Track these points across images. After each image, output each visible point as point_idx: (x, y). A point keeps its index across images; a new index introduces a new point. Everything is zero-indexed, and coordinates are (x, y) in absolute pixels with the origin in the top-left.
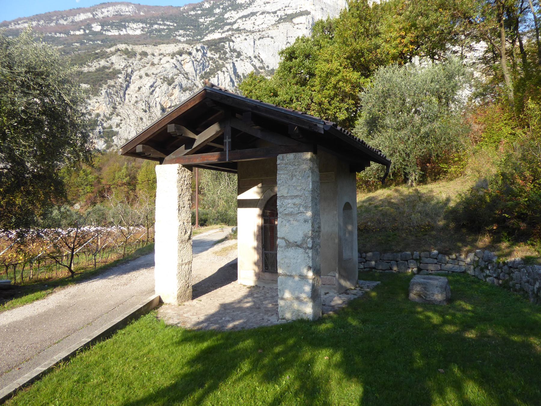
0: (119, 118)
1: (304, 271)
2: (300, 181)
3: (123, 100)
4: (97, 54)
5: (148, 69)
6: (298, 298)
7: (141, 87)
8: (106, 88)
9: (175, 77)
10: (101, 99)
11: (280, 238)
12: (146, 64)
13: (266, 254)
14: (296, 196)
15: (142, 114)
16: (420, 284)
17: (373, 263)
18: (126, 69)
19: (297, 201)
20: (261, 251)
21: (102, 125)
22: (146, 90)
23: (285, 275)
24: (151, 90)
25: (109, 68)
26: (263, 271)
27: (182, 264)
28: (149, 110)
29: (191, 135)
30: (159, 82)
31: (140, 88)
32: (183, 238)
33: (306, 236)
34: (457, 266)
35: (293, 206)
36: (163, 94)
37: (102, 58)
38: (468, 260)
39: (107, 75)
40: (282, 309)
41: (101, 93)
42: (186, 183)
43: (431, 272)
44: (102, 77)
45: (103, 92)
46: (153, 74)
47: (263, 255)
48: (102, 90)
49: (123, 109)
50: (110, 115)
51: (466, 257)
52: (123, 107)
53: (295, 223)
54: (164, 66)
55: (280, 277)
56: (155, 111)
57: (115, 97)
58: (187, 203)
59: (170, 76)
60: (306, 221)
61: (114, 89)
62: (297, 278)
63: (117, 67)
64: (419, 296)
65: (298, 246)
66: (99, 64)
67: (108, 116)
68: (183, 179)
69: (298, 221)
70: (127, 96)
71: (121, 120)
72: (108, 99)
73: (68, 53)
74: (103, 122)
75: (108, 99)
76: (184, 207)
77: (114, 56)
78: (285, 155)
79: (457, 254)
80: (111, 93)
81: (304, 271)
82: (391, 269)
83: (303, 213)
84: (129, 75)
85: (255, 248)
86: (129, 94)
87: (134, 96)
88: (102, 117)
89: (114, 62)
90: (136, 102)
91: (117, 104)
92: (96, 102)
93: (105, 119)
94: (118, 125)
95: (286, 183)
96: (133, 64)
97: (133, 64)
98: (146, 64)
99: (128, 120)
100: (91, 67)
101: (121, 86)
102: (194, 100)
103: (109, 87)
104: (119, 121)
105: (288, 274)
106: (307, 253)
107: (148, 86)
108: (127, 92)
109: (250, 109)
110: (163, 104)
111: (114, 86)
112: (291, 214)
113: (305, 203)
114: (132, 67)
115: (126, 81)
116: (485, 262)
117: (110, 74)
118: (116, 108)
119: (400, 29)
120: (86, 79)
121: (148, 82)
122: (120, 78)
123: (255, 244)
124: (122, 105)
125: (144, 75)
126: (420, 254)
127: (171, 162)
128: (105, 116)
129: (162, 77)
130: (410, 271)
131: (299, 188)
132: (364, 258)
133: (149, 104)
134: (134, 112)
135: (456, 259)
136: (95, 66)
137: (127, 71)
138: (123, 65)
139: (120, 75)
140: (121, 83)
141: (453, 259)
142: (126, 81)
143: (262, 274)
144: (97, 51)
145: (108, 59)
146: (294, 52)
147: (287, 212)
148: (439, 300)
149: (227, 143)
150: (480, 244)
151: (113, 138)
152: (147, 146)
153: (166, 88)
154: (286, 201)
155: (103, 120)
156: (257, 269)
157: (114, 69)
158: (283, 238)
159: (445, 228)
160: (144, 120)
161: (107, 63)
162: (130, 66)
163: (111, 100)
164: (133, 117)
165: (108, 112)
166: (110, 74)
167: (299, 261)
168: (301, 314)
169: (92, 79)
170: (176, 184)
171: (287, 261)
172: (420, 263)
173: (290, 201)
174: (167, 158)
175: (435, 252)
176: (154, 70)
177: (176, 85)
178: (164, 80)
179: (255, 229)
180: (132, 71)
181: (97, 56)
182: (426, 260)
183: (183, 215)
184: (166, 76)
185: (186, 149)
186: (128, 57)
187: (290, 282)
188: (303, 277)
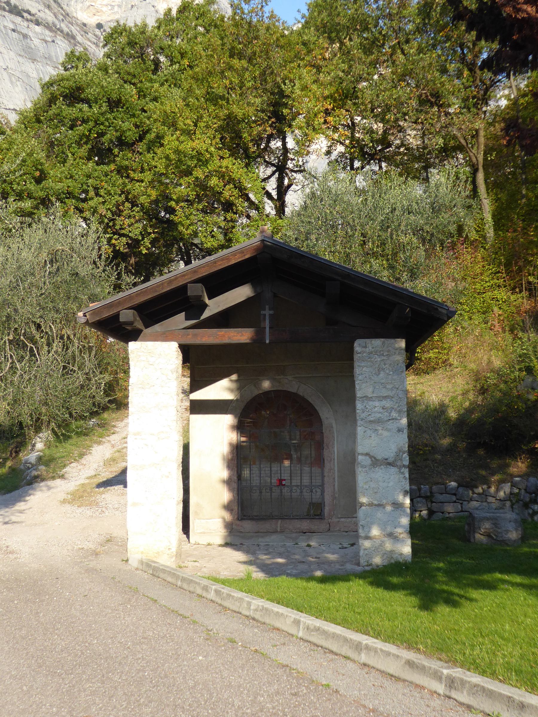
1: (401, 498)
2: (390, 377)
6: (391, 535)
11: (362, 454)
14: (385, 398)
16: (488, 519)
19: (388, 404)
20: (235, 485)
23: (371, 505)
26: (238, 519)
33: (400, 450)
34: (485, 504)
35: (381, 410)
38: (501, 494)
40: (366, 552)
43: (447, 515)
51: (498, 490)
53: (386, 433)
55: (363, 508)
60: (400, 430)
62: (389, 508)
64: (489, 536)
65: (390, 464)
69: (388, 430)
78: (368, 341)
79: (485, 487)
81: (401, 498)
83: (396, 419)
85: (224, 482)
95: (370, 378)
102: (242, 252)
105: (376, 502)
106: (403, 473)
109: (340, 278)
112: (379, 421)
113: (399, 407)
116: (531, 494)
119: (325, 98)
123: (225, 474)
126: (431, 488)
127: (165, 337)
130: (417, 515)
131: (389, 387)
135: (483, 494)
141: (479, 494)
143: (238, 522)
146: (80, 89)
147: (372, 419)
149: (267, 317)
150: (513, 470)
154: (371, 403)
156: (227, 516)
158: (367, 454)
159: (451, 449)
167: (391, 484)
168: (395, 556)
171: (372, 485)
172: (432, 502)
173: (377, 404)
174: (147, 331)
175: (453, 484)
179: (225, 449)
182: (441, 498)
185: (187, 319)
187: (379, 514)
188: (397, 506)
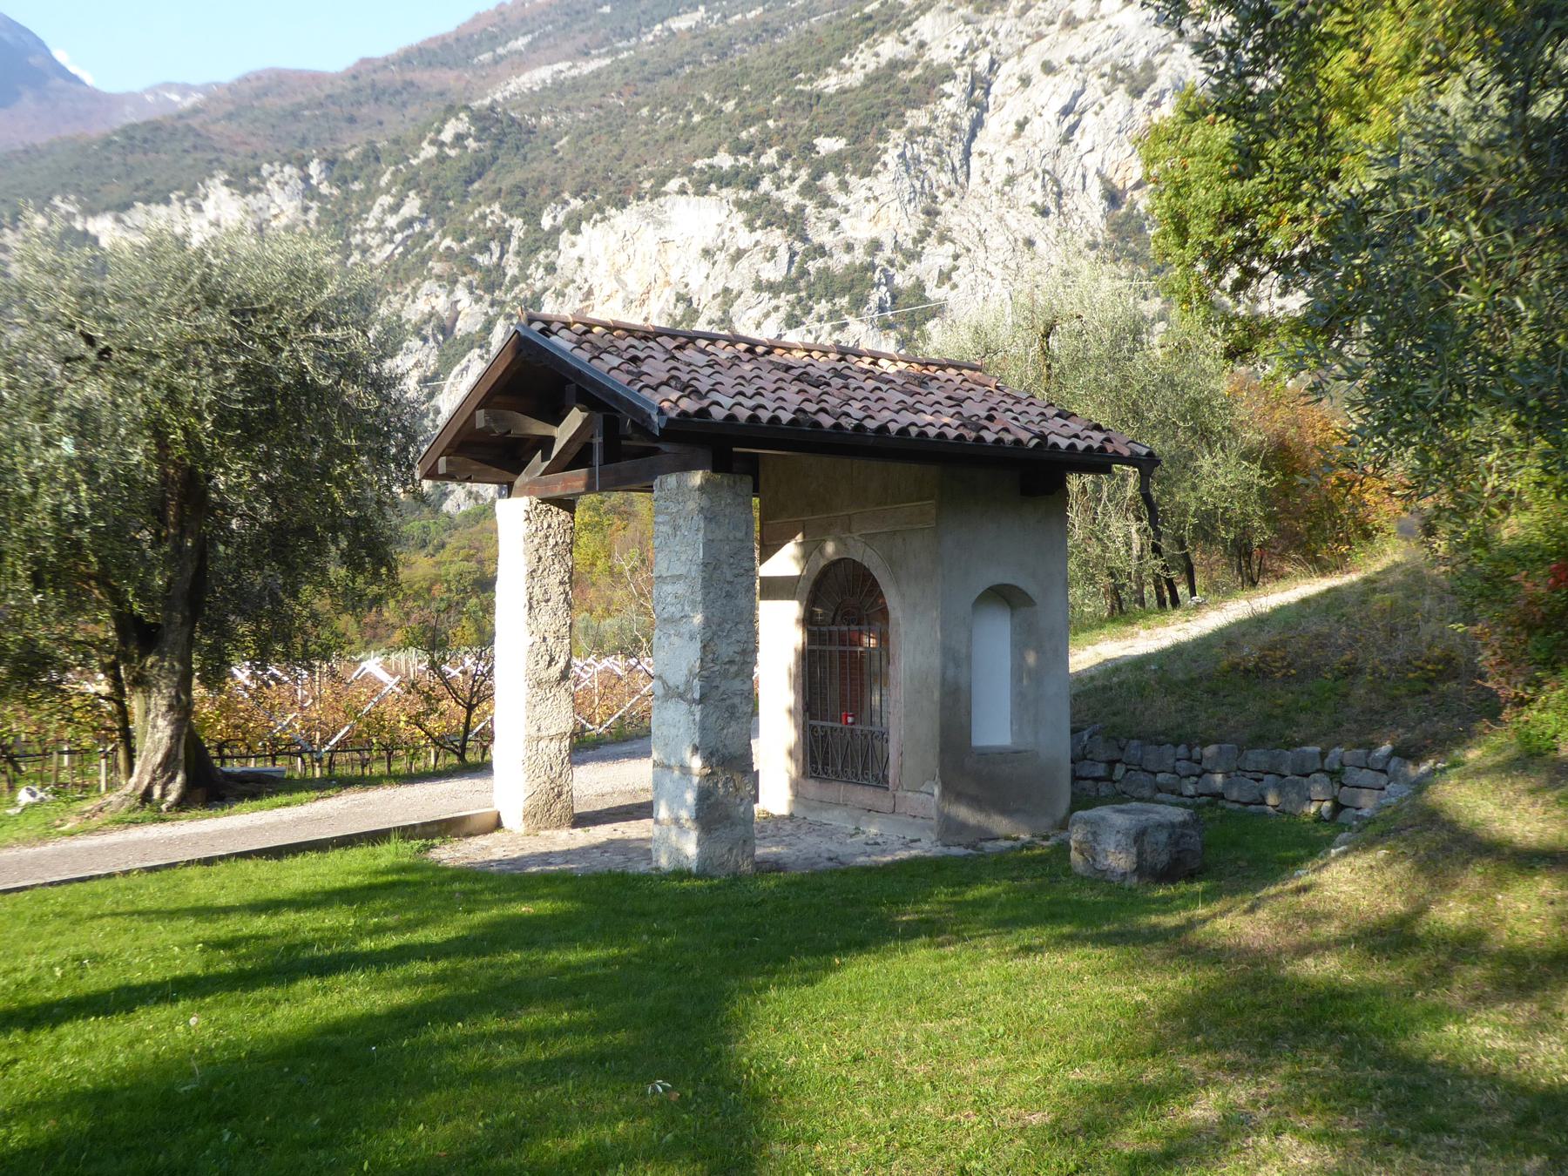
0: (949, 248)
1: (687, 754)
3: (962, 179)
4: (869, 18)
5: (1053, 46)
7: (1026, 120)
8: (901, 141)
9: (1158, 59)
10: (882, 183)
12: (1043, 28)
13: (813, 728)
15: (1031, 225)
17: (1219, 778)
18: (970, 59)
19: (680, 588)
21: (889, 279)
22: (1045, 130)
24: (1065, 126)
25: (908, 65)
27: (539, 739)
28: (1059, 206)
29: (538, 428)
30: (1096, 87)
31: (1021, 126)
32: (544, 675)
36: (1112, 135)
37: (886, 32)
39: (905, 91)
41: (885, 164)
42: (552, 541)
44: (887, 103)
45: (891, 157)
46: (1071, 61)
47: (804, 731)
48: (885, 151)
49: (963, 213)
50: (915, 241)
52: (962, 205)
53: (674, 639)
54: (1113, 21)
56: (1083, 207)
57: (931, 171)
58: (556, 592)
59: (1138, 60)
61: (930, 140)
62: (677, 773)
63: (939, 55)
66: (877, 55)
67: (909, 245)
68: (541, 534)
70: (975, 161)
71: (956, 257)
72: (907, 182)
73: (776, 31)
74: (892, 271)
75: (907, 182)
76: (547, 601)
77: (928, 15)
80: (917, 159)
82: (1263, 803)
84: (983, 80)
85: (790, 711)
86: (981, 154)
87: (1000, 161)
88: (887, 252)
89: (927, 37)
90: (1011, 180)
91: (941, 197)
92: (867, 200)
93: (899, 258)
94: (944, 277)
96: (995, 34)
97: (995, 34)
98: (1043, 28)
99: (981, 254)
100: (848, 70)
101: (954, 128)
103: (911, 135)
104: (949, 262)
107: (1051, 114)
108: (976, 147)
110: (1110, 173)
111: (927, 131)
114: (993, 46)
115: (971, 104)
117: (914, 86)
118: (938, 213)
120: (834, 118)
121: (1051, 94)
122: (950, 96)
124: (956, 199)
125: (1037, 73)
128: (897, 246)
129: (1107, 68)
132: (1199, 762)
133: (1057, 182)
134: (1001, 219)
136: (864, 62)
137: (973, 65)
138: (961, 42)
139: (947, 87)
140: (954, 115)
142: (971, 104)
144: (867, 10)
145: (906, 32)
148: (1120, 871)
151: (929, 325)
152: (460, 459)
153: (1122, 110)
155: (891, 263)
157: (928, 66)
160: (1041, 245)
161: (902, 48)
162: (985, 44)
163: (918, 185)
164: (997, 240)
165: (909, 227)
166: (914, 86)
169: (853, 114)
170: (522, 546)
172: (1343, 785)
176: (1075, 44)
177: (1163, 93)
178: (1116, 81)
180: (993, 62)
181: (869, 25)
183: (544, 619)
184: (1121, 62)
185: (543, 460)
186: (979, 10)
188: (685, 770)
